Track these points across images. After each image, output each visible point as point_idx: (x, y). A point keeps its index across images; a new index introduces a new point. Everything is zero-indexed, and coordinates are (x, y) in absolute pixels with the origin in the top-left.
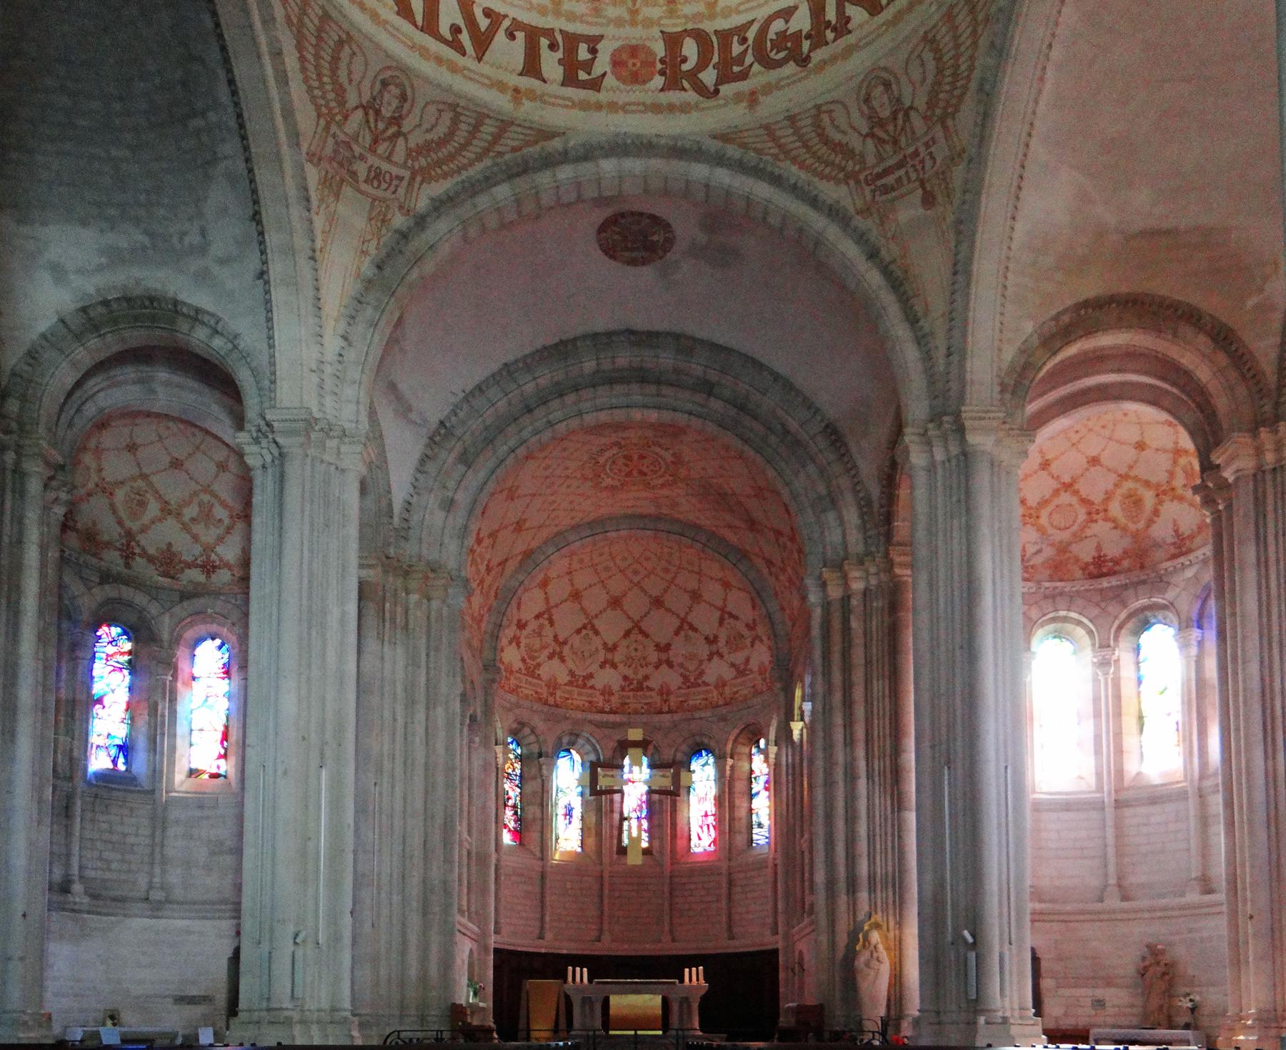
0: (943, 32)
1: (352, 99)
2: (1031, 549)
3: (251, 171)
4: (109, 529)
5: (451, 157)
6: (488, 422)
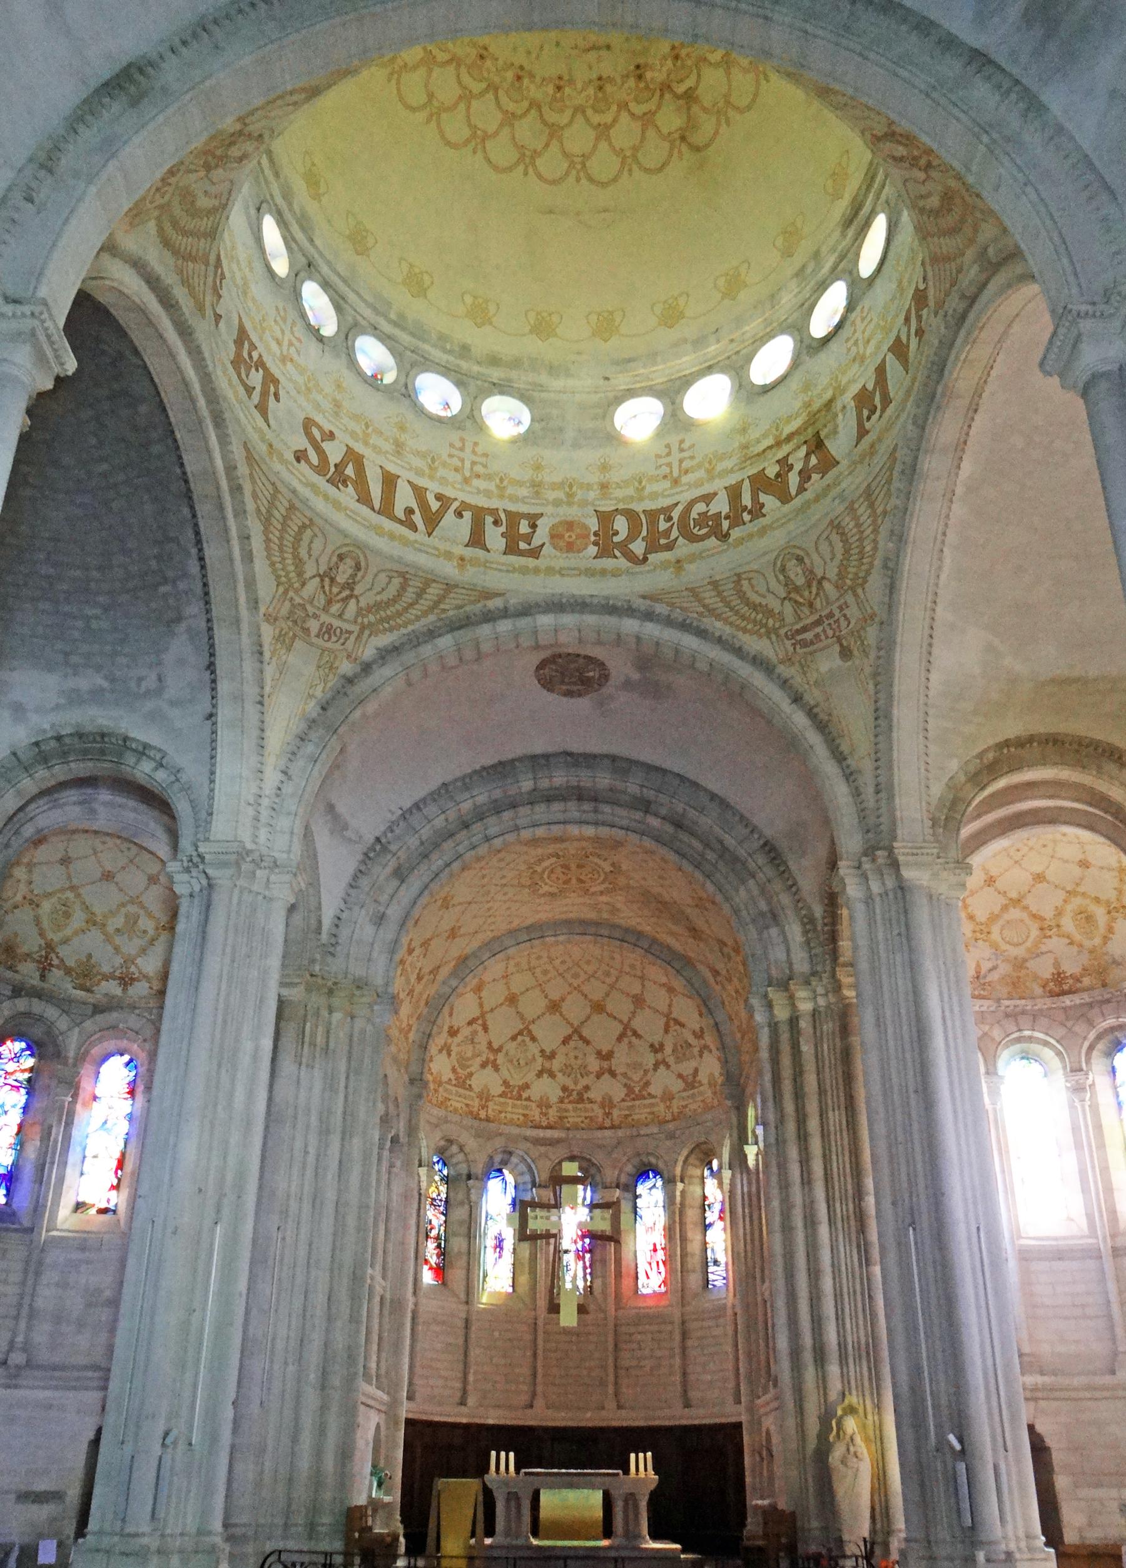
0: (849, 523)
1: (310, 570)
2: (986, 966)
3: (210, 629)
4: (31, 943)
5: (399, 614)
6: (424, 838)
